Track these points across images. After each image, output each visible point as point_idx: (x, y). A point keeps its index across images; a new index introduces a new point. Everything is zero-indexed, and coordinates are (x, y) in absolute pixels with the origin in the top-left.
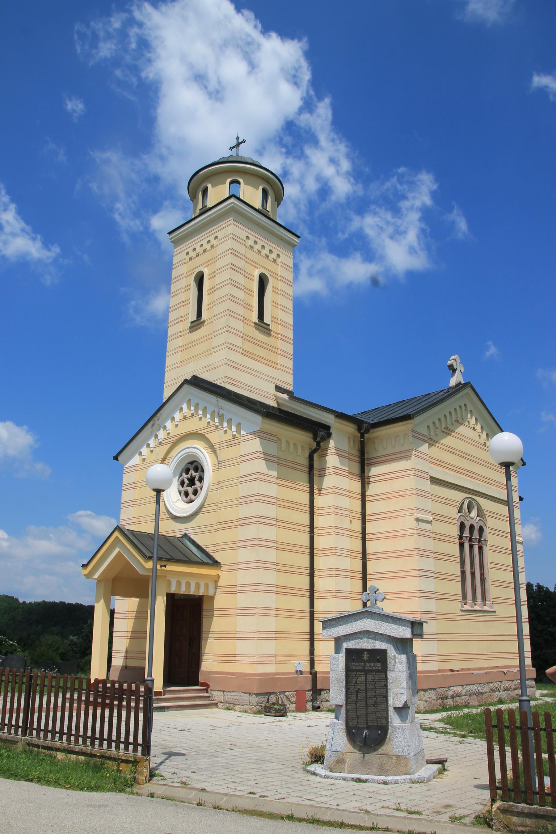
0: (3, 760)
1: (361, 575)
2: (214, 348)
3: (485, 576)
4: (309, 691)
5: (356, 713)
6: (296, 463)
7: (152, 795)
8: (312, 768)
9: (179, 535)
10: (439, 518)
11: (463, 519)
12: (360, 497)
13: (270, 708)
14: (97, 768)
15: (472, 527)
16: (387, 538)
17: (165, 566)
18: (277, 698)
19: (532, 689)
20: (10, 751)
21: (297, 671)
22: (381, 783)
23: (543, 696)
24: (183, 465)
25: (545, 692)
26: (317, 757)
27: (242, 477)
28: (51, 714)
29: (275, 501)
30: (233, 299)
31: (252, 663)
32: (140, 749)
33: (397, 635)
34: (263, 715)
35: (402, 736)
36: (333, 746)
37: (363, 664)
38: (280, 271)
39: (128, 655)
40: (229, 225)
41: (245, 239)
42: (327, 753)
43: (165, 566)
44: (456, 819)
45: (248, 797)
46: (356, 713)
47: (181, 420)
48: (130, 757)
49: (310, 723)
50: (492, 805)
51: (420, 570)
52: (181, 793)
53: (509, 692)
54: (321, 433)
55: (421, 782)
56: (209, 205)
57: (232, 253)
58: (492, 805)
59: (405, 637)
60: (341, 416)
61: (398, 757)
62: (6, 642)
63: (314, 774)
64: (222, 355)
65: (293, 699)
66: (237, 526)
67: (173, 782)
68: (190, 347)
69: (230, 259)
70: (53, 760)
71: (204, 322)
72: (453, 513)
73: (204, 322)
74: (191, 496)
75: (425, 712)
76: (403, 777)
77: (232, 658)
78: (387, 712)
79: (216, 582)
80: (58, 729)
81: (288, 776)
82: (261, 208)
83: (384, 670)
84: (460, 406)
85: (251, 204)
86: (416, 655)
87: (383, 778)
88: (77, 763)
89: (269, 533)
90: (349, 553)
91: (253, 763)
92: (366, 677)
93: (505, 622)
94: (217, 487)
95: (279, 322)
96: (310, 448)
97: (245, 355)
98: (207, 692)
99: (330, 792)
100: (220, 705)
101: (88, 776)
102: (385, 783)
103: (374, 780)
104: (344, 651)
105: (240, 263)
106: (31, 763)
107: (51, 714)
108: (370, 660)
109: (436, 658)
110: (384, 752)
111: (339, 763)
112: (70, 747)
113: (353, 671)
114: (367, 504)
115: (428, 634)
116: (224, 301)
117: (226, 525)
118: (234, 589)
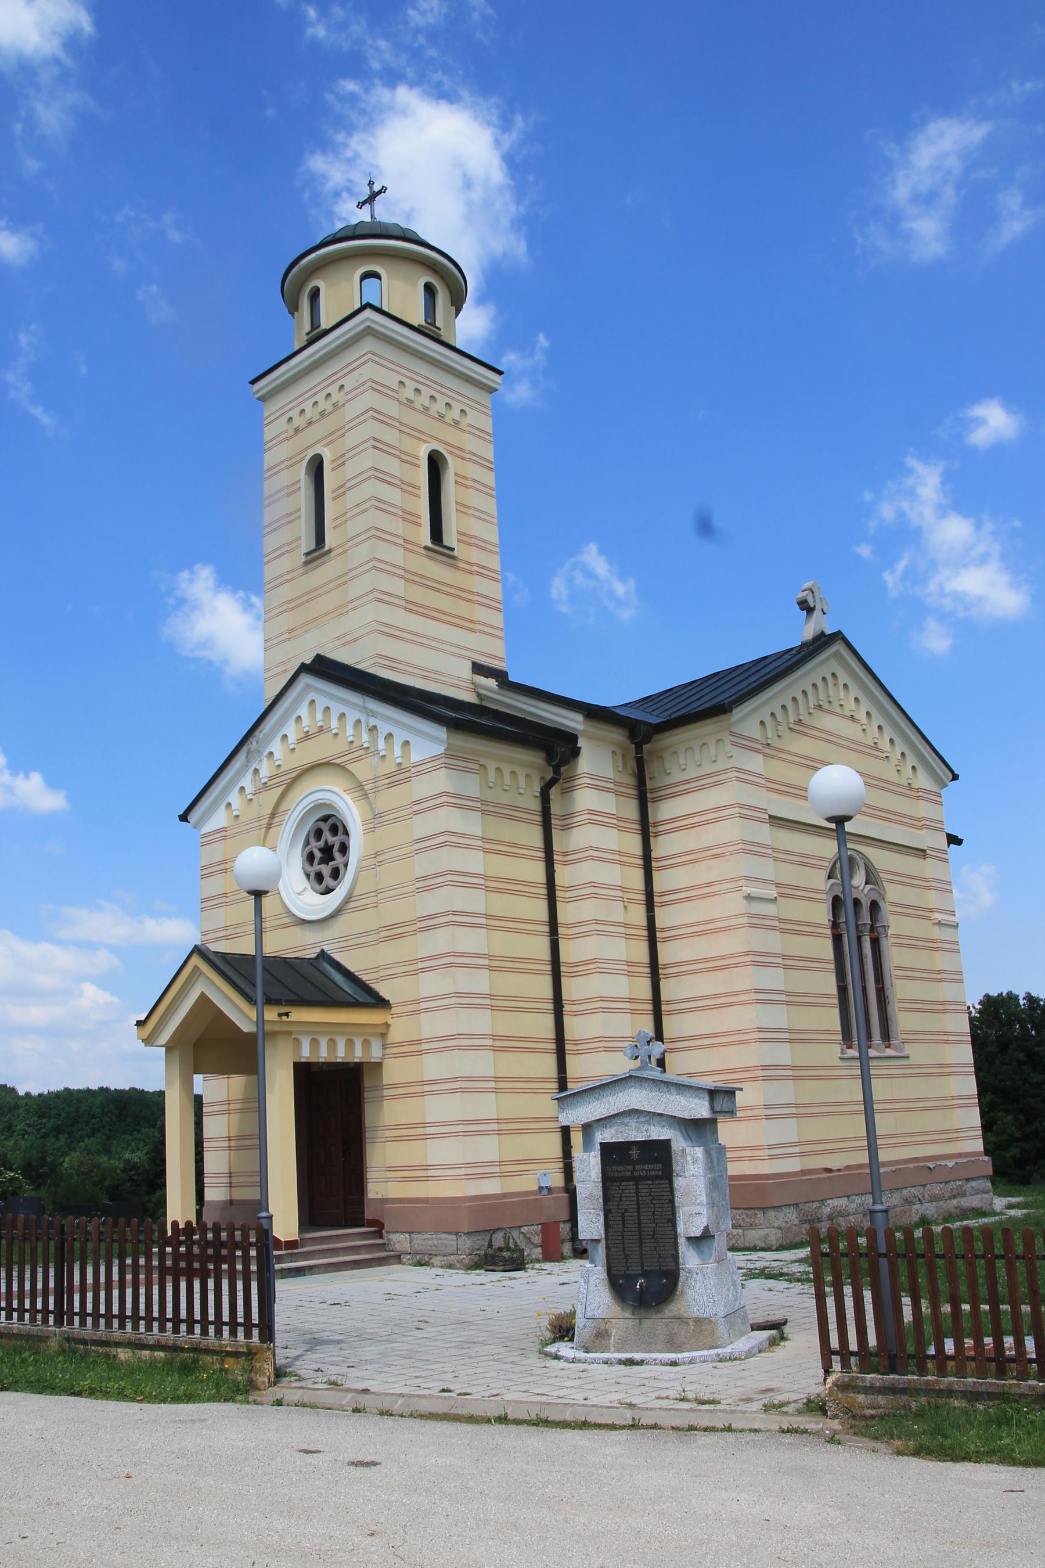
0: (27, 1367)
1: (650, 1007)
2: (353, 601)
3: (888, 993)
4: (564, 1222)
5: (624, 1251)
6: (517, 809)
7: (279, 1403)
8: (552, 1349)
9: (311, 953)
10: (787, 891)
11: (838, 892)
12: (641, 862)
13: (493, 1257)
14: (187, 1369)
15: (857, 902)
16: (695, 934)
17: (287, 1014)
18: (506, 1238)
19: (985, 1196)
20: (37, 1353)
21: (541, 1188)
22: (666, 1364)
23: (1010, 1207)
25: (1014, 1200)
26: (563, 1330)
27: (419, 841)
28: (102, 1294)
29: (482, 881)
30: (382, 506)
31: (457, 1178)
32: (255, 1332)
33: (686, 1115)
34: (483, 1271)
35: (705, 1284)
36: (588, 1309)
37: (630, 1167)
38: (470, 443)
39: (234, 1180)
40: (364, 363)
41: (396, 386)
42: (579, 1322)
43: (287, 1014)
44: (774, 1406)
45: (438, 1397)
46: (624, 1251)
48: (241, 1346)
49: (565, 1278)
50: (825, 1380)
51: (758, 991)
52: (331, 1397)
53: (941, 1203)
54: (561, 749)
55: (735, 1359)
56: (325, 325)
57: (374, 418)
58: (825, 1380)
59: (699, 1116)
60: (594, 713)
61: (698, 1321)
63: (557, 1357)
64: (368, 614)
65: (537, 1240)
66: (415, 932)
67: (315, 1383)
68: (308, 601)
69: (371, 429)
70: (112, 1362)
71: (330, 551)
72: (818, 880)
73: (330, 551)
74: (328, 881)
75: (781, 1248)
76: (705, 1352)
77: (422, 1171)
78: (676, 1245)
79: (383, 1035)
80: (116, 1310)
81: (512, 1363)
82: (423, 323)
83: (667, 1174)
84: (824, 679)
85: (404, 319)
86: (724, 1147)
87: (672, 1356)
88: (153, 1362)
89: (472, 941)
90: (625, 967)
91: (455, 1347)
92: (637, 1188)
93: (930, 1075)
94: (373, 861)
95: (473, 541)
96: (542, 778)
97: (410, 611)
98: (381, 1237)
99: (578, 1382)
100: (405, 1258)
101: (171, 1381)
102: (674, 1364)
103: (655, 1360)
104: (598, 1147)
105: (390, 436)
106: (75, 1369)
107: (102, 1294)
108: (642, 1161)
109: (796, 1150)
110: (675, 1313)
111: (600, 1337)
112: (139, 1339)
113: (615, 1179)
114: (655, 875)
115: (745, 1108)
116: (365, 511)
117: (394, 932)
118: (416, 1047)
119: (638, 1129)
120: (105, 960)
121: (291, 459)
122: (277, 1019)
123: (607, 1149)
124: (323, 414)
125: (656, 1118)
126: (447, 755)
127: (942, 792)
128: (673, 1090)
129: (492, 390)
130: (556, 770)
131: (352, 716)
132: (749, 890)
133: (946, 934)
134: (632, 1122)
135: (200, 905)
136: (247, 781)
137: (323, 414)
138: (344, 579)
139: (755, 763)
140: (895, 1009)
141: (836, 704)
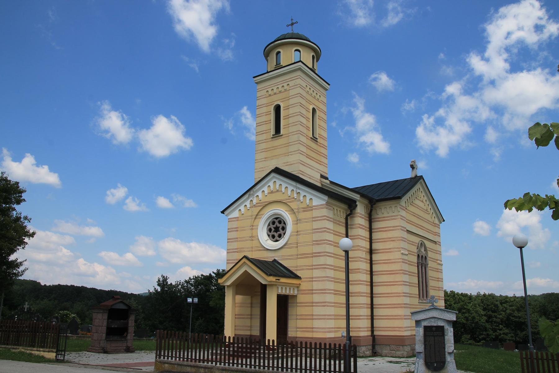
15: (422, 256)
16: (384, 263)
41: (305, 87)
47: (269, 193)
62: (70, 315)
74: (277, 238)
78: (445, 355)
79: (298, 287)
105: (304, 102)
119: (434, 322)
120: (68, 240)
123: (426, 328)
124: (280, 92)
129: (326, 90)
130: (351, 211)
131: (290, 188)
134: (433, 320)
135: (227, 241)
136: (248, 203)
137: (280, 92)
138: (288, 145)
139: (403, 213)
140: (429, 288)
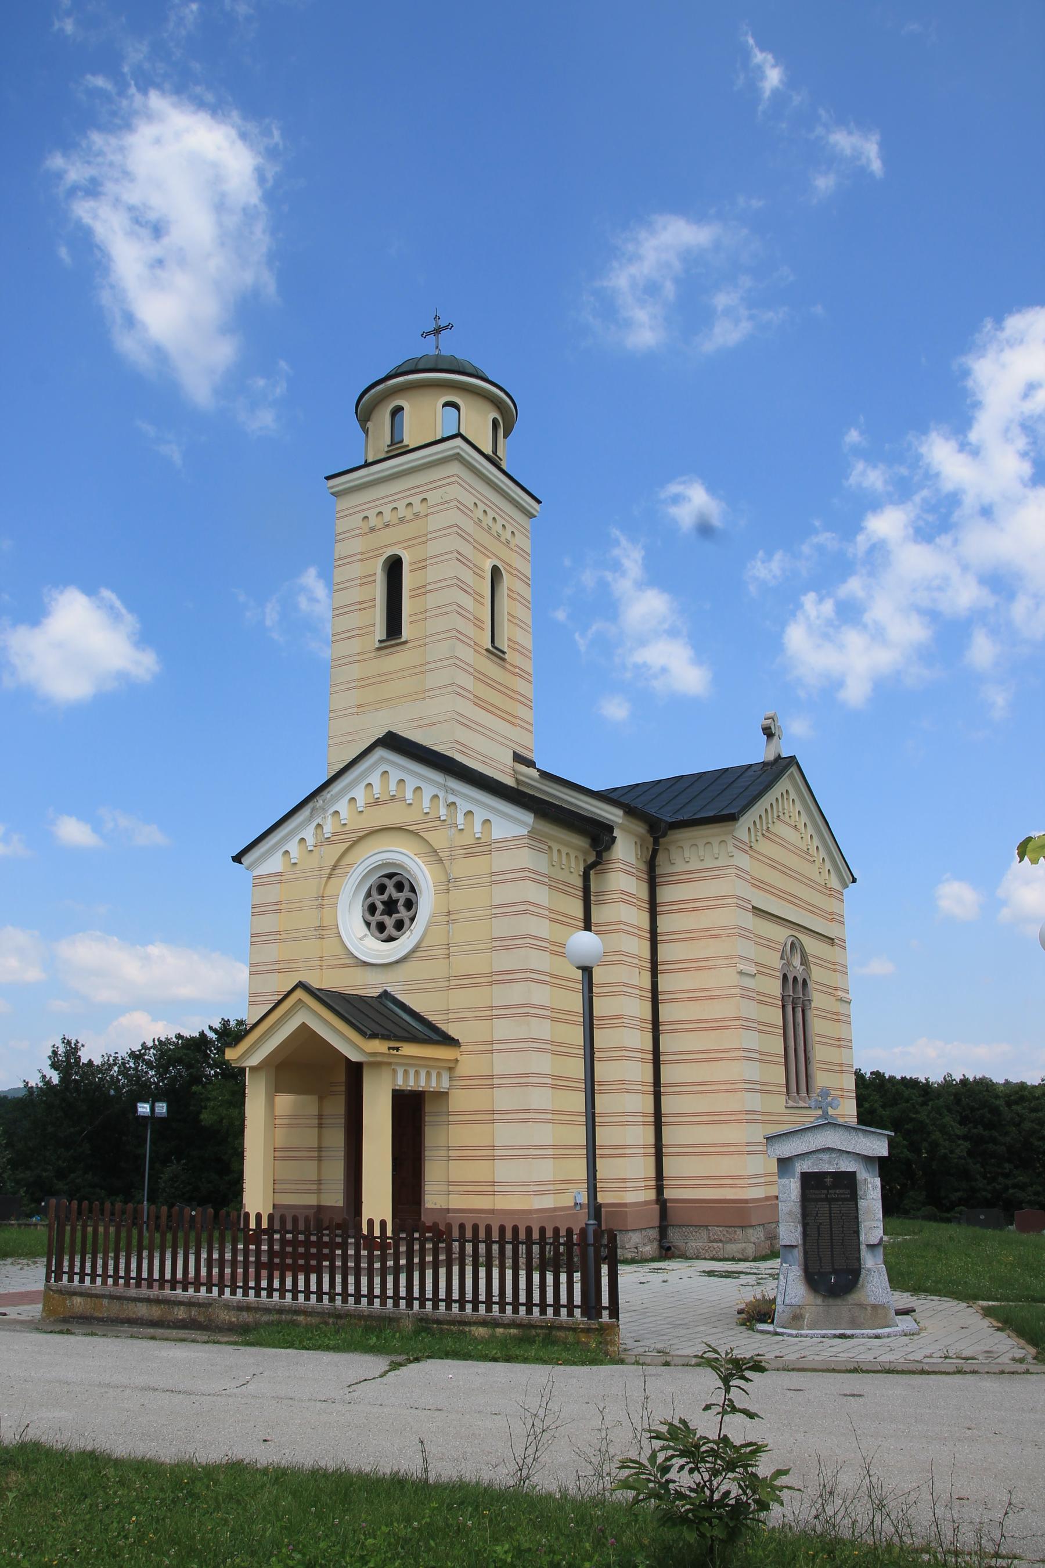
1: (651, 1057)
6: (568, 884)
9: (374, 993)
15: (795, 979)
16: (690, 999)
17: (397, 1049)
24: (373, 880)
37: (825, 1191)
40: (450, 484)
42: (779, 1307)
43: (397, 1049)
47: (368, 805)
61: (875, 1307)
68: (379, 683)
71: (406, 642)
79: (451, 1069)
82: (491, 453)
95: (517, 647)
102: (877, 1337)
104: (798, 1175)
105: (467, 550)
108: (835, 1186)
109: (762, 1180)
111: (796, 1319)
116: (445, 613)
119: (830, 1163)
121: (364, 553)
122: (386, 1051)
125: (845, 1155)
126: (530, 837)
127: (845, 891)
128: (860, 1134)
129: (531, 516)
130: (599, 855)
132: (741, 967)
133: (841, 1008)
134: (825, 1156)
136: (309, 834)
137: (402, 520)
139: (743, 860)
140: (815, 1066)
141: (787, 816)
